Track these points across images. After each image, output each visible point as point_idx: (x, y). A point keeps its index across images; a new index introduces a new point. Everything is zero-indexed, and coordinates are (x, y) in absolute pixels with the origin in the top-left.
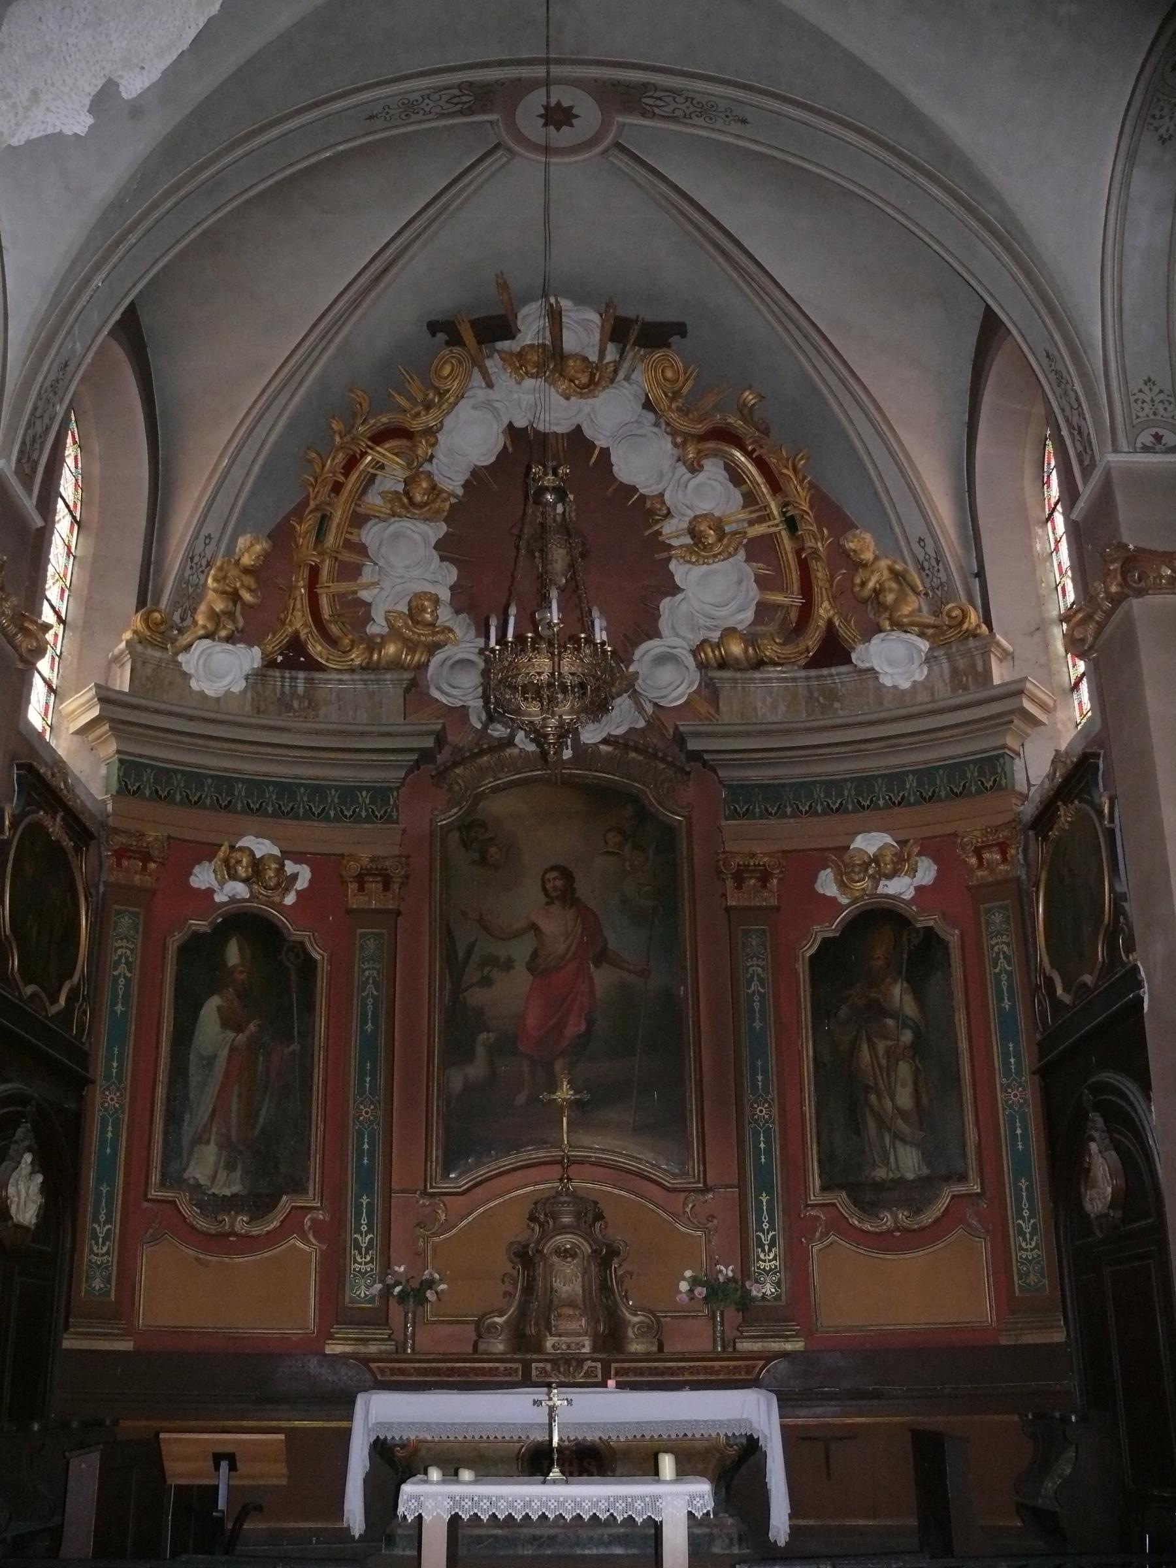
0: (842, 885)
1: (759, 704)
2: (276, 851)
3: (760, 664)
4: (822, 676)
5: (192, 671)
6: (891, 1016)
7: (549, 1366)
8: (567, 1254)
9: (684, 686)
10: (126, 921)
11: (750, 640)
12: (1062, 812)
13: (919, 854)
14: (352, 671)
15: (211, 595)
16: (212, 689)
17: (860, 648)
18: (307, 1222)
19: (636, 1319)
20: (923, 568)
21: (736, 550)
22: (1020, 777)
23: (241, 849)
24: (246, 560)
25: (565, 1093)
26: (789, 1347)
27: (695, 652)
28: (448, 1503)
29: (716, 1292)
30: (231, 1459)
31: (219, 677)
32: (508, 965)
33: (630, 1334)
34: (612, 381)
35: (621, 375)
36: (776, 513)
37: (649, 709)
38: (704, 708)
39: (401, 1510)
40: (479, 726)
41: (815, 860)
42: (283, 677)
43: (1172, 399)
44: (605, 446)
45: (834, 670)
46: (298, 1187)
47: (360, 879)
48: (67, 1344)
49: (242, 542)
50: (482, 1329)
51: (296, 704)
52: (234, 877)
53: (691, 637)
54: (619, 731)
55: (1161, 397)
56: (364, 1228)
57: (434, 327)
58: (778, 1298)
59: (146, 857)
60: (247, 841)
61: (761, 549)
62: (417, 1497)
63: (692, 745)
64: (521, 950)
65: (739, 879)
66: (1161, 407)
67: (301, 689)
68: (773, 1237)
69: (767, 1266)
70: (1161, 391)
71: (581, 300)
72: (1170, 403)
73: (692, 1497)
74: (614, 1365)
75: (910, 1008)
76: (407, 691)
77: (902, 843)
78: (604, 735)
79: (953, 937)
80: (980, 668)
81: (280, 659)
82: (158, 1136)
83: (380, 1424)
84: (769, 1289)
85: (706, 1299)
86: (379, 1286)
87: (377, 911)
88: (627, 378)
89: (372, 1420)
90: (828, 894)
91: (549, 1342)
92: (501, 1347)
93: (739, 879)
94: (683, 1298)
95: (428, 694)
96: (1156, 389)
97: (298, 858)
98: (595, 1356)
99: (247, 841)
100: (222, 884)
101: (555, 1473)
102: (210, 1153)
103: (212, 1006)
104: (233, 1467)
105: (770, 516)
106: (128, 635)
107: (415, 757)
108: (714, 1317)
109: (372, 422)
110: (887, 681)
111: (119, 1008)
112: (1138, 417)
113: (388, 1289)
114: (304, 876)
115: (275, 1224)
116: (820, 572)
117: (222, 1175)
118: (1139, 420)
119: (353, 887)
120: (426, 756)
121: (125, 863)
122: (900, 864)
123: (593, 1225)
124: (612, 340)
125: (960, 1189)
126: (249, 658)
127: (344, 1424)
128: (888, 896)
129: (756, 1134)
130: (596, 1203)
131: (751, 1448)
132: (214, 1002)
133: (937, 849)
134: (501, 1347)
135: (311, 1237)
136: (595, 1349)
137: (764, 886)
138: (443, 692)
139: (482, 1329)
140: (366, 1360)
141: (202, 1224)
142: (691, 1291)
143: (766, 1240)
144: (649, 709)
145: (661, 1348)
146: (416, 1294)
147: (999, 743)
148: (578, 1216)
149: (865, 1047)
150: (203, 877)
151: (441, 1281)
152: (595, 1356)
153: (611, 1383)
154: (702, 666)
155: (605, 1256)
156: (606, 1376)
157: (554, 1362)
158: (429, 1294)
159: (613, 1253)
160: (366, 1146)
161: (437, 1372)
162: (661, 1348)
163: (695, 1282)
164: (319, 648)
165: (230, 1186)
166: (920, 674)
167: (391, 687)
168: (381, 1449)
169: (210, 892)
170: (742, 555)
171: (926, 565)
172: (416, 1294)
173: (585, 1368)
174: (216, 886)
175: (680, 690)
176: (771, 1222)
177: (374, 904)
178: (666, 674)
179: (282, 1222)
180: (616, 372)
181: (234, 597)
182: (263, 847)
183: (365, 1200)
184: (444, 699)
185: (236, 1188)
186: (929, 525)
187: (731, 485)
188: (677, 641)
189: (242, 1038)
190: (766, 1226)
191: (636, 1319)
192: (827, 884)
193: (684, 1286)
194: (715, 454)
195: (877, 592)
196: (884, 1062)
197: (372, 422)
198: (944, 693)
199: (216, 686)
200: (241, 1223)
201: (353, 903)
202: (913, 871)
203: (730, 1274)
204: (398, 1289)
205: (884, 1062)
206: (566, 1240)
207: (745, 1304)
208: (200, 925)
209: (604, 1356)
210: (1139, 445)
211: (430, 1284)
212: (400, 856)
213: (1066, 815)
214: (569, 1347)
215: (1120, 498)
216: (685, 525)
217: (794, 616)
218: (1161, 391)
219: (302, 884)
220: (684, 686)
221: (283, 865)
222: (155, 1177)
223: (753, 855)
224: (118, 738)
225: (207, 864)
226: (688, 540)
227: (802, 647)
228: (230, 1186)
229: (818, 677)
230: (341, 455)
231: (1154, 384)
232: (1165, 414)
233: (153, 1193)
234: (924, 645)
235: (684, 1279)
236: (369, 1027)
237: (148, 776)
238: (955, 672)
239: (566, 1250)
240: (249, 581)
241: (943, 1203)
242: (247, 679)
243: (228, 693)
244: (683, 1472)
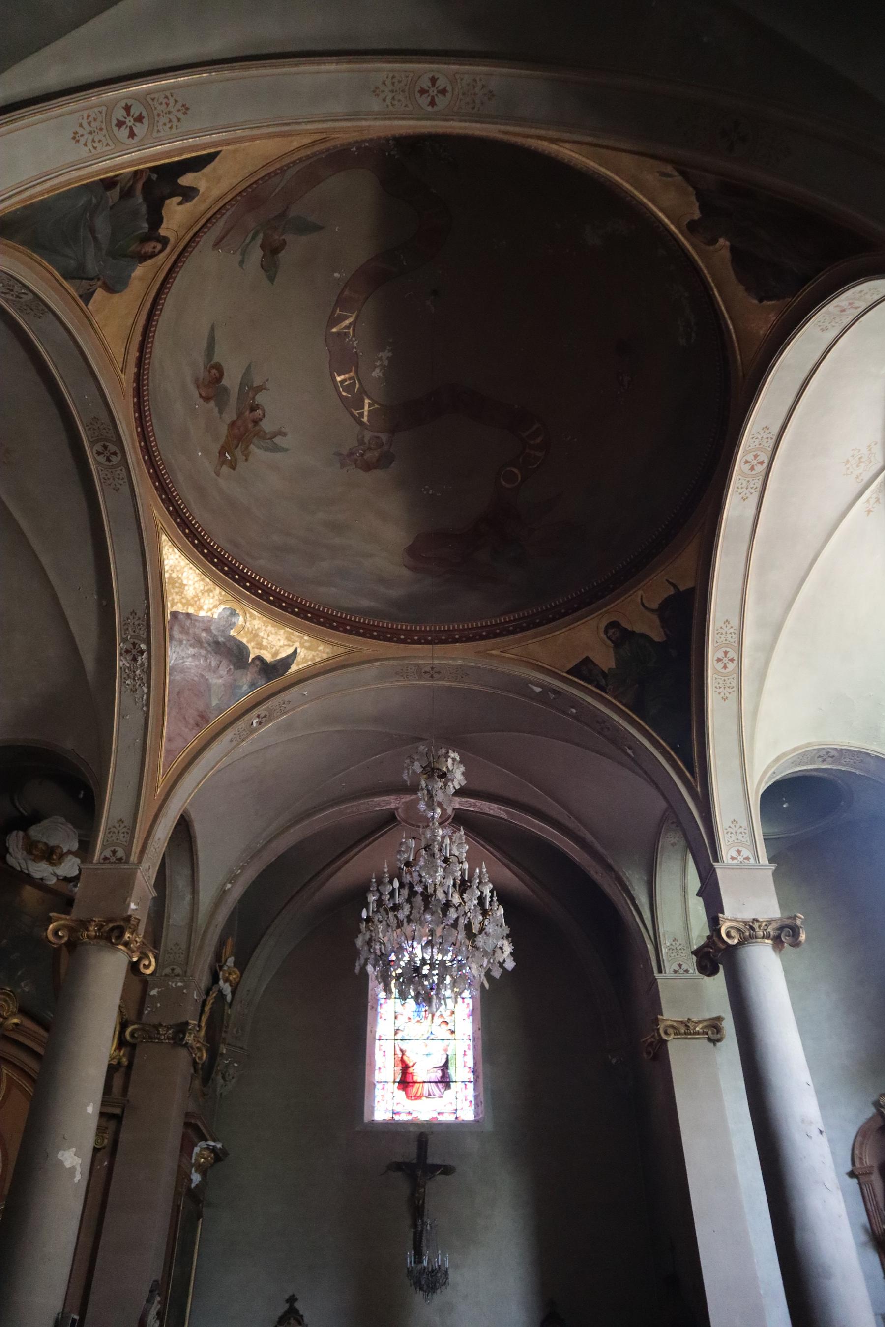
55: (680, 947)
70: (125, 827)
218: (125, 827)
232: (161, 123)
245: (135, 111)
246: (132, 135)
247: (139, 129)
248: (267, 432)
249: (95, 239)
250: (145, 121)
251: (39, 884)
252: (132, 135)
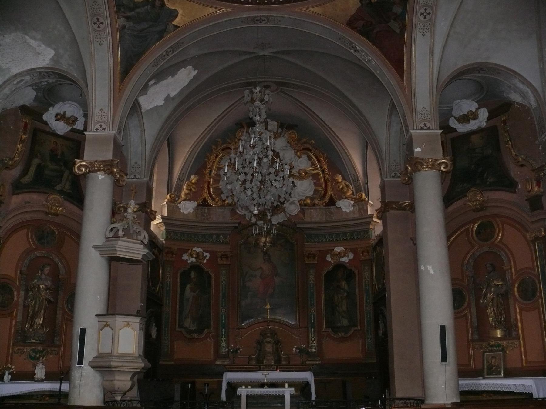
0: (332, 258)
1: (314, 215)
2: (202, 251)
3: (314, 205)
4: (329, 208)
5: (181, 208)
6: (342, 289)
7: (265, 367)
8: (268, 342)
9: (297, 210)
10: (169, 268)
11: (312, 198)
12: (378, 248)
13: (350, 252)
14: (218, 207)
15: (185, 190)
16: (186, 212)
17: (338, 202)
18: (211, 335)
19: (284, 356)
20: (354, 181)
21: (309, 177)
22: (373, 234)
23: (194, 251)
24: (193, 181)
25: (268, 306)
26: (317, 363)
27: (299, 201)
28: (246, 392)
29: (301, 351)
30: (208, 384)
31: (188, 209)
33: (282, 360)
34: (280, 137)
35: (282, 135)
36: (319, 167)
37: (288, 215)
38: (301, 215)
39: (238, 393)
40: (248, 220)
41: (326, 253)
42: (202, 208)
43: (430, 113)
44: (278, 151)
45: (332, 207)
46: (208, 327)
47: (221, 257)
48: (160, 363)
49: (192, 177)
50: (250, 359)
51: (205, 215)
52: (192, 257)
53: (298, 197)
54: (281, 221)
55: (398, 164)
56: (223, 337)
57: (237, 124)
58: (315, 352)
59: (173, 254)
60: (194, 249)
61: (315, 176)
62: (240, 391)
63: (298, 226)
65: (308, 257)
66: (397, 167)
67: (206, 211)
68: (315, 339)
69: (313, 345)
71: (272, 119)
72: (429, 114)
73: (291, 391)
74: (279, 367)
75: (346, 287)
76: (231, 211)
77: (346, 249)
78: (277, 222)
79: (356, 272)
80: (365, 208)
81: (201, 204)
82: (177, 317)
83: (229, 379)
84: (313, 350)
85: (299, 352)
86: (227, 349)
87: (225, 264)
88: (283, 136)
89: (227, 378)
90: (329, 260)
91: (265, 361)
92: (254, 363)
93: (308, 257)
94: (294, 352)
95: (236, 211)
96: (425, 110)
97: (207, 252)
98: (275, 364)
99: (194, 249)
100: (190, 258)
101: (266, 386)
102: (189, 320)
103: (188, 287)
104: (208, 386)
105: (317, 169)
106: (166, 200)
107: (233, 228)
108: (301, 356)
109: (222, 146)
110: (344, 210)
111: (168, 288)
112: (420, 119)
113: (229, 350)
114: (208, 255)
115: (204, 336)
116: (329, 184)
118: (421, 120)
119: (219, 259)
120: (236, 228)
121: (168, 255)
122: (345, 254)
123: (274, 336)
124: (280, 127)
125: (355, 329)
126: (194, 204)
127: (222, 379)
128: (342, 262)
129: (311, 315)
130: (275, 331)
131: (308, 384)
133: (354, 251)
134: (254, 363)
135: (211, 338)
136: (274, 363)
137: (314, 259)
138: (239, 211)
139: (250, 359)
140: (225, 366)
141: (188, 336)
142: (296, 350)
143: (313, 339)
144: (288, 215)
145: (289, 362)
146: (236, 351)
147: (368, 227)
148: (271, 334)
149: (336, 296)
150: (185, 257)
151: (241, 348)
152: (275, 364)
153: (278, 370)
154: (301, 205)
155: (277, 343)
156: (277, 369)
157: (266, 365)
158: (239, 351)
159: (279, 342)
160: (223, 318)
161: (240, 368)
162: (289, 362)
163: (297, 348)
164: (210, 201)
165: (193, 327)
166: (351, 209)
167: (227, 211)
168: (229, 384)
169: (187, 260)
170: (311, 178)
171: (355, 180)
172: (236, 351)
173: (273, 367)
174: (188, 259)
175: (295, 211)
176: (314, 335)
177: (224, 263)
178: (292, 207)
179: (206, 335)
180: (281, 135)
181: (191, 190)
182: (199, 250)
183: (223, 330)
184: (240, 213)
185: (195, 328)
186: (355, 172)
187: (308, 161)
188: (295, 199)
189: (195, 294)
190: (313, 336)
191: (284, 356)
192: (329, 258)
193: (294, 349)
194: (304, 153)
195: (343, 188)
196: (340, 300)
197: (222, 146)
198: (357, 215)
199: (187, 211)
200: (196, 336)
201: (220, 262)
202: (348, 256)
203: (304, 347)
204: (232, 350)
205: (340, 300)
206: (268, 339)
207: (308, 353)
208: (185, 268)
209: (277, 364)
210: (391, 176)
211: (239, 349)
212: (230, 251)
213: (378, 249)
214: (269, 362)
215: (386, 188)
216: (297, 170)
217: (323, 192)
218: (427, 111)
219: (207, 258)
220: (297, 210)
221: (203, 254)
222: (177, 326)
223: (312, 251)
224: (165, 226)
225: (186, 254)
226: (298, 175)
227: (324, 201)
228: (193, 327)
229: (328, 209)
230: (215, 154)
231: (425, 109)
233: (177, 329)
234: (352, 202)
235: (294, 348)
236: (224, 291)
237: (172, 234)
238: (359, 209)
239: (268, 342)
240: (194, 186)
241: (351, 332)
242: (194, 209)
243: (189, 213)
244: (290, 386)
245: (95, 21)
246: (102, 23)
247: (101, 20)
248: (14, 196)
249: (148, 28)
250: (99, 17)
251: (480, 131)
252: (102, 23)
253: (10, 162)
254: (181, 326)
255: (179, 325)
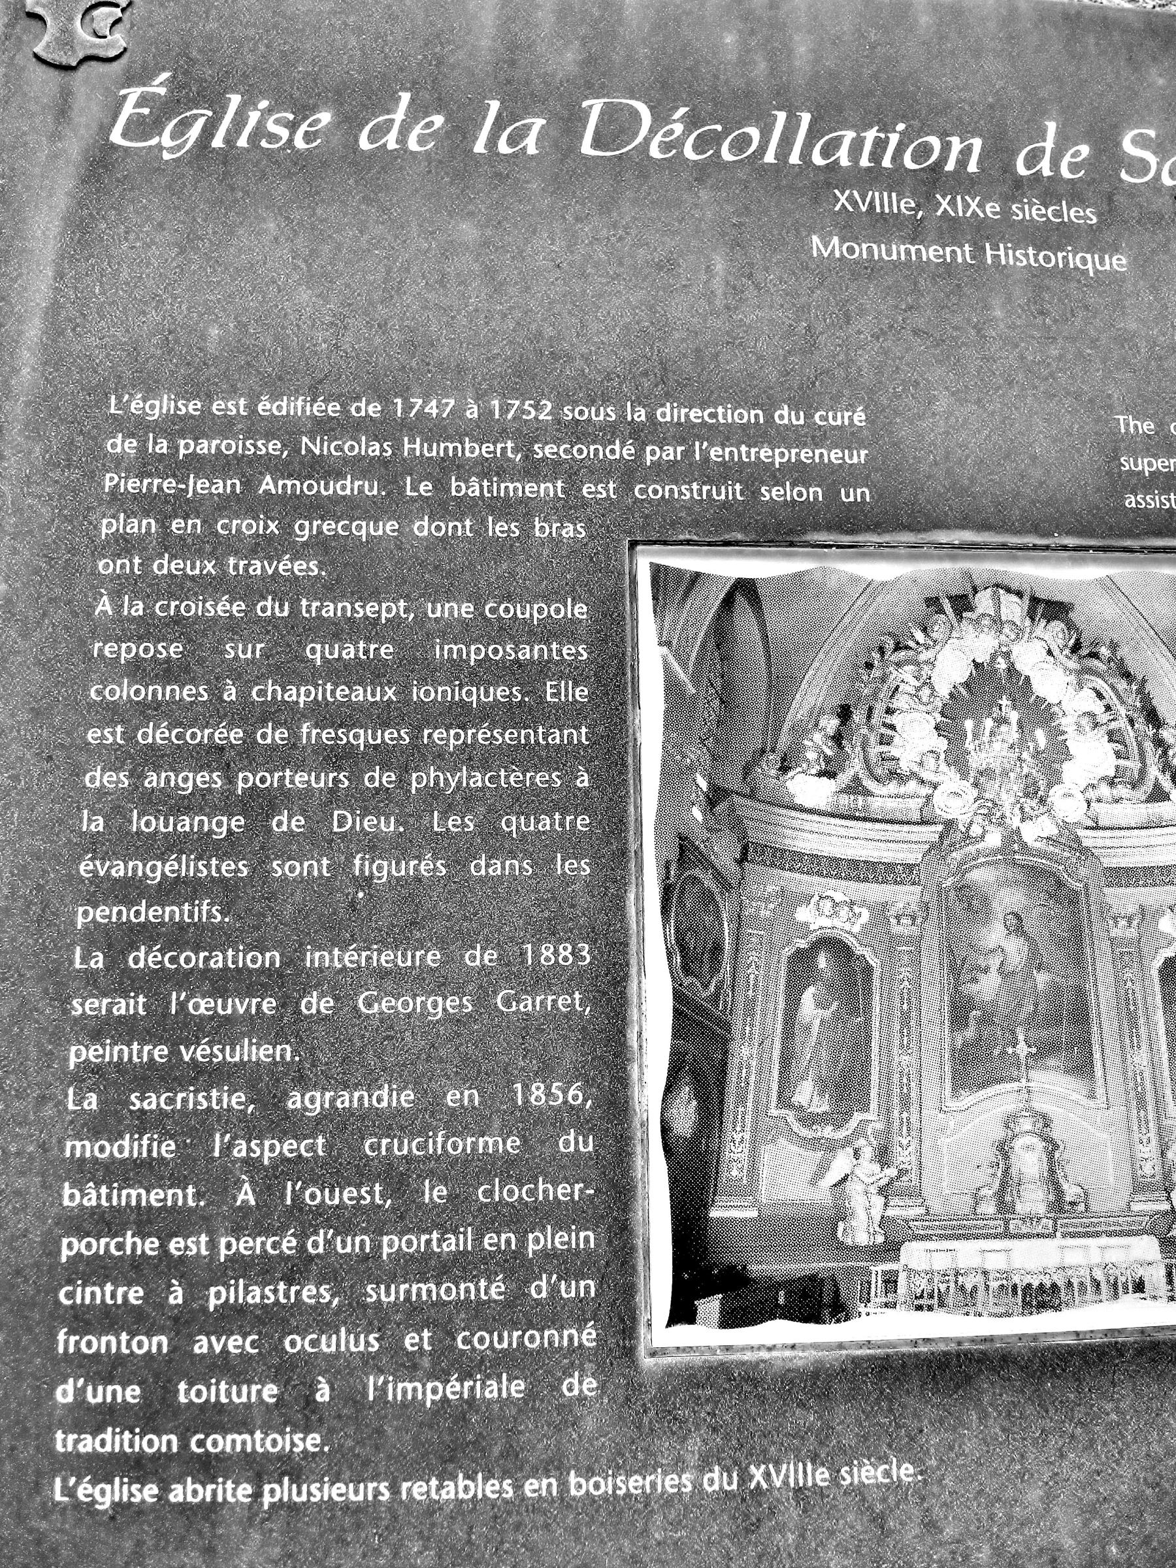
32: (986, 970)
50: (977, 1199)
64: (994, 962)
103: (808, 997)
117: (816, 1098)
132: (811, 990)
139: (977, 1199)
155: (1052, 1147)
165: (821, 1106)
185: (826, 1108)
200: (828, 1131)
228: (821, 1106)
253: (728, 40)
254: (784, 1100)
255: (779, 1098)
